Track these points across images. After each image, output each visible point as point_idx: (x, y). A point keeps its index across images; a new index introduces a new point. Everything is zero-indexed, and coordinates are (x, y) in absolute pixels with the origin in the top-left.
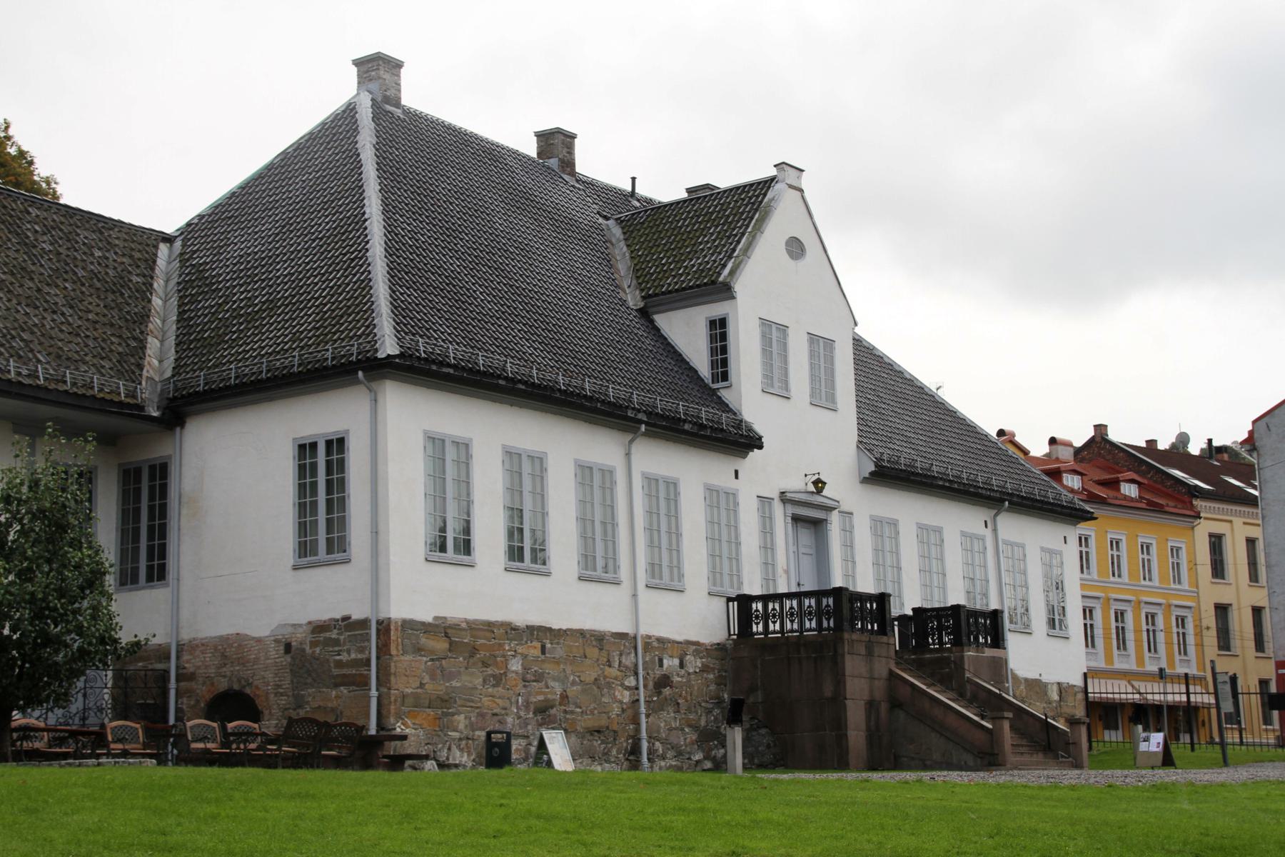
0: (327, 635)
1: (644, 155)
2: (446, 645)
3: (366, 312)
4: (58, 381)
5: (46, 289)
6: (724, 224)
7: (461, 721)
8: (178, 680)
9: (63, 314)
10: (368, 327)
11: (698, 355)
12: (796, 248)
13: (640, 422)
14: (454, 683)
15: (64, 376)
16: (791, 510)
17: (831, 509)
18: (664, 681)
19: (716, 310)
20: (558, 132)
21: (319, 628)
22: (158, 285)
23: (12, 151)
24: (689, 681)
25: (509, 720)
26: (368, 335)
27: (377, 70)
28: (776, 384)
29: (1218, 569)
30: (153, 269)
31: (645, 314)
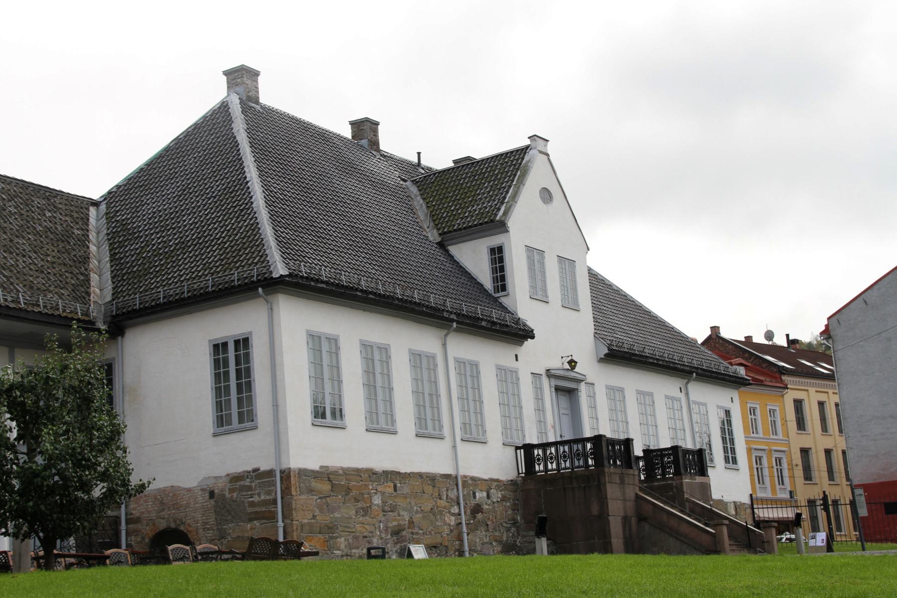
0: (242, 483)
1: (431, 135)
2: (329, 487)
3: (258, 246)
4: (33, 305)
5: (16, 240)
6: (494, 180)
7: (342, 542)
8: (127, 523)
9: (30, 257)
10: (261, 256)
11: (483, 274)
12: (546, 195)
13: (452, 321)
14: (337, 515)
15: (38, 301)
16: (554, 382)
18: (477, 509)
20: (367, 120)
21: (236, 478)
22: (92, 236)
24: (494, 508)
26: (263, 262)
27: (241, 78)
28: (539, 295)
29: (801, 424)
30: (88, 225)
31: (442, 245)
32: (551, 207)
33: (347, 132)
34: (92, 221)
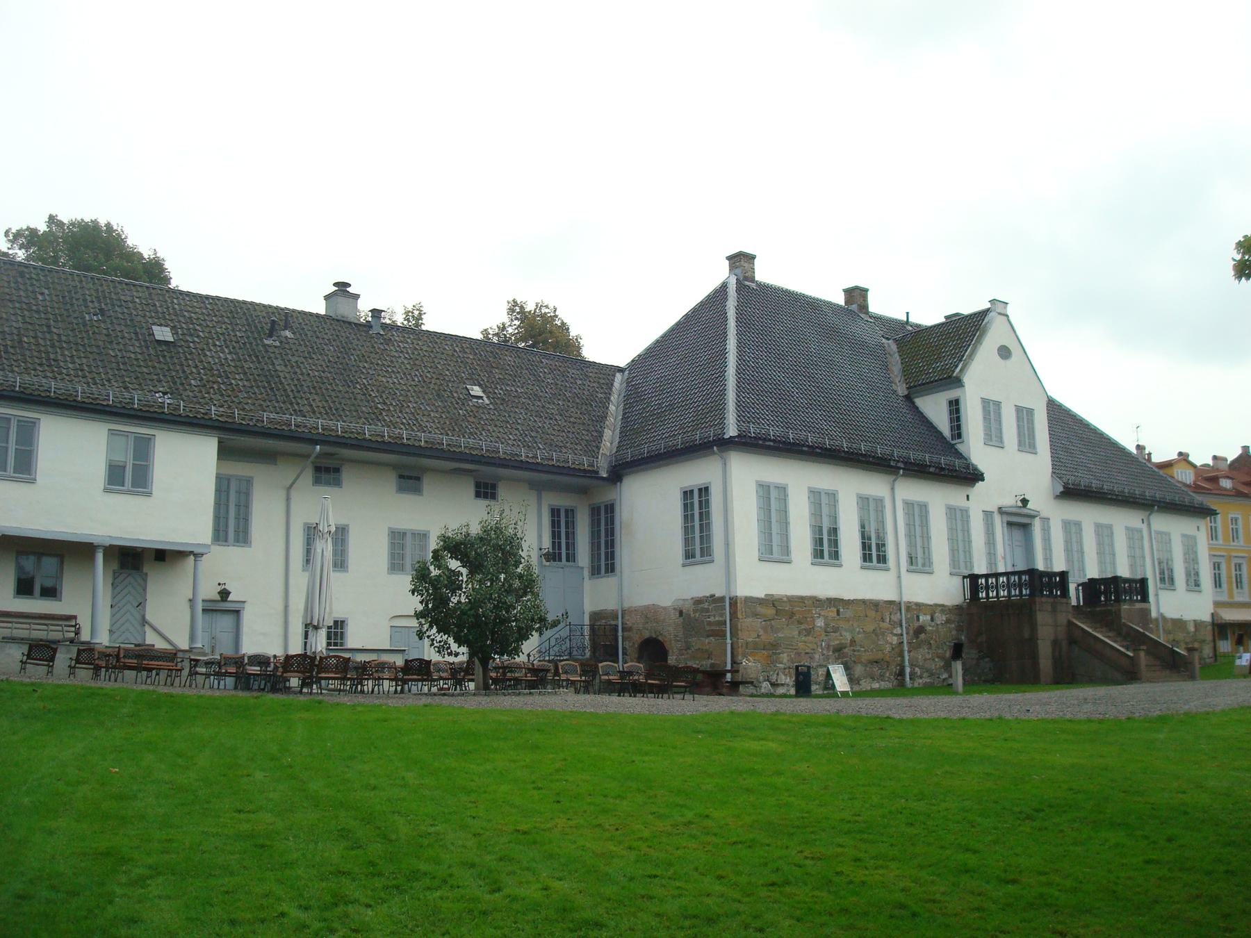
1: (915, 297)
2: (774, 612)
7: (785, 658)
11: (942, 422)
12: (1005, 352)
13: (900, 468)
14: (780, 635)
16: (1006, 518)
17: (1034, 517)
18: (920, 630)
19: (952, 394)
20: (857, 288)
21: (698, 601)
22: (614, 398)
23: (559, 323)
25: (817, 656)
27: (741, 261)
28: (994, 437)
31: (909, 398)
32: (1008, 362)
33: (840, 300)
34: (617, 384)
